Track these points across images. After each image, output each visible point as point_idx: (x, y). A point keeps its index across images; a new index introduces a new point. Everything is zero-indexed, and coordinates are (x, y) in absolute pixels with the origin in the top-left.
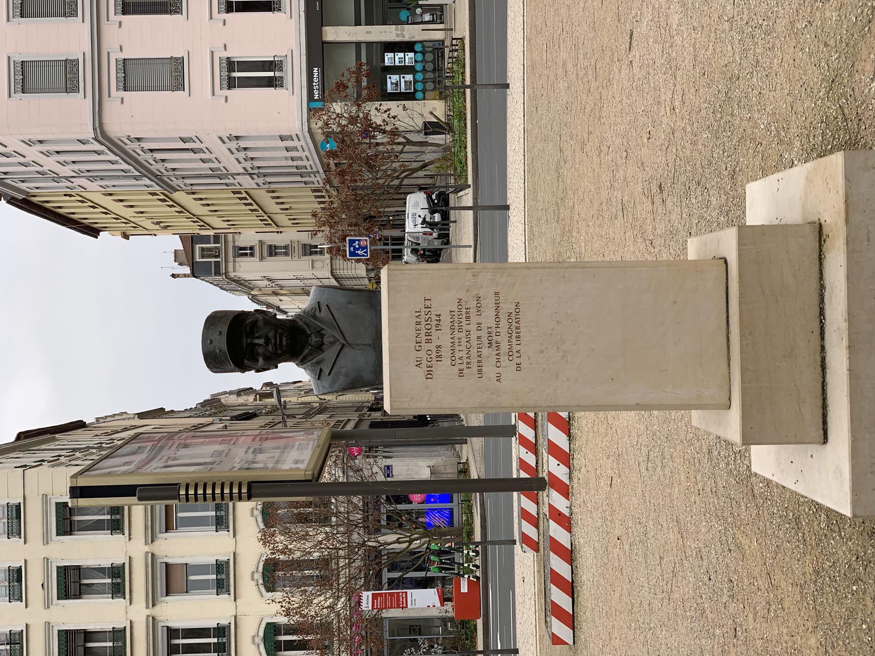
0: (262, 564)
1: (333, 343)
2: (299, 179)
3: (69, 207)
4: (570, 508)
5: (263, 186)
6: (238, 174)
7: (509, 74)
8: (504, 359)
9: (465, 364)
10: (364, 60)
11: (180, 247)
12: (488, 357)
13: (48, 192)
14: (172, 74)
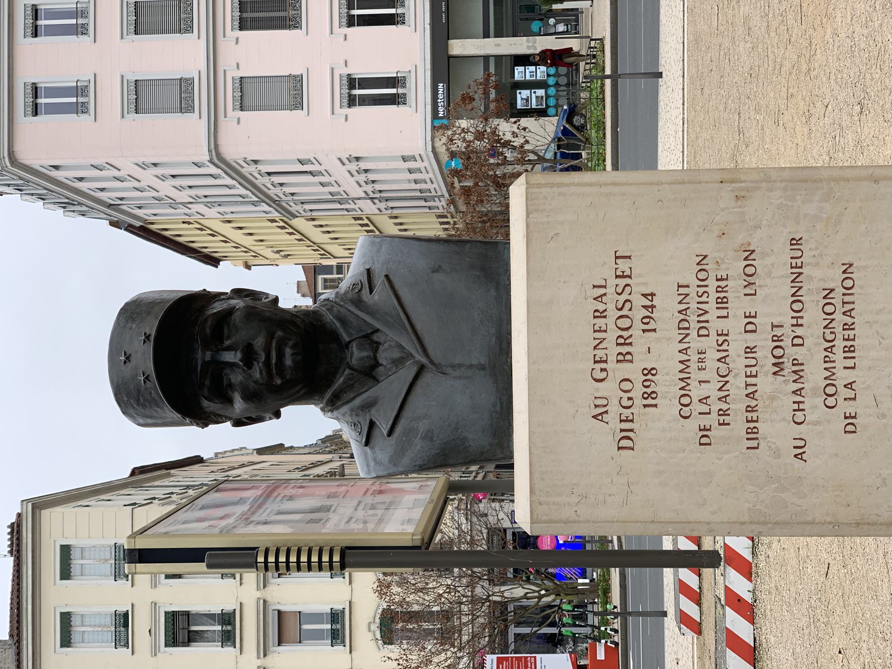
0: (378, 616)
1: (398, 362)
2: (423, 203)
3: (188, 235)
4: (754, 592)
5: (384, 212)
6: (359, 199)
7: (662, 61)
8: (814, 403)
9: (714, 415)
10: (492, 70)
11: (302, 278)
12: (773, 398)
13: (166, 220)
14: (291, 92)
